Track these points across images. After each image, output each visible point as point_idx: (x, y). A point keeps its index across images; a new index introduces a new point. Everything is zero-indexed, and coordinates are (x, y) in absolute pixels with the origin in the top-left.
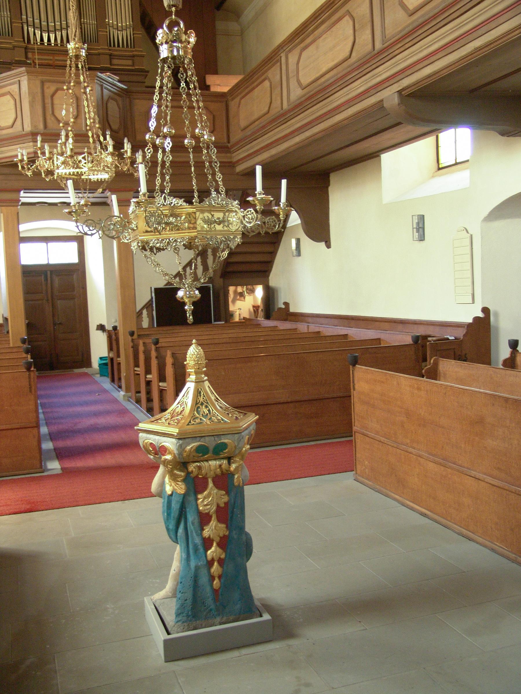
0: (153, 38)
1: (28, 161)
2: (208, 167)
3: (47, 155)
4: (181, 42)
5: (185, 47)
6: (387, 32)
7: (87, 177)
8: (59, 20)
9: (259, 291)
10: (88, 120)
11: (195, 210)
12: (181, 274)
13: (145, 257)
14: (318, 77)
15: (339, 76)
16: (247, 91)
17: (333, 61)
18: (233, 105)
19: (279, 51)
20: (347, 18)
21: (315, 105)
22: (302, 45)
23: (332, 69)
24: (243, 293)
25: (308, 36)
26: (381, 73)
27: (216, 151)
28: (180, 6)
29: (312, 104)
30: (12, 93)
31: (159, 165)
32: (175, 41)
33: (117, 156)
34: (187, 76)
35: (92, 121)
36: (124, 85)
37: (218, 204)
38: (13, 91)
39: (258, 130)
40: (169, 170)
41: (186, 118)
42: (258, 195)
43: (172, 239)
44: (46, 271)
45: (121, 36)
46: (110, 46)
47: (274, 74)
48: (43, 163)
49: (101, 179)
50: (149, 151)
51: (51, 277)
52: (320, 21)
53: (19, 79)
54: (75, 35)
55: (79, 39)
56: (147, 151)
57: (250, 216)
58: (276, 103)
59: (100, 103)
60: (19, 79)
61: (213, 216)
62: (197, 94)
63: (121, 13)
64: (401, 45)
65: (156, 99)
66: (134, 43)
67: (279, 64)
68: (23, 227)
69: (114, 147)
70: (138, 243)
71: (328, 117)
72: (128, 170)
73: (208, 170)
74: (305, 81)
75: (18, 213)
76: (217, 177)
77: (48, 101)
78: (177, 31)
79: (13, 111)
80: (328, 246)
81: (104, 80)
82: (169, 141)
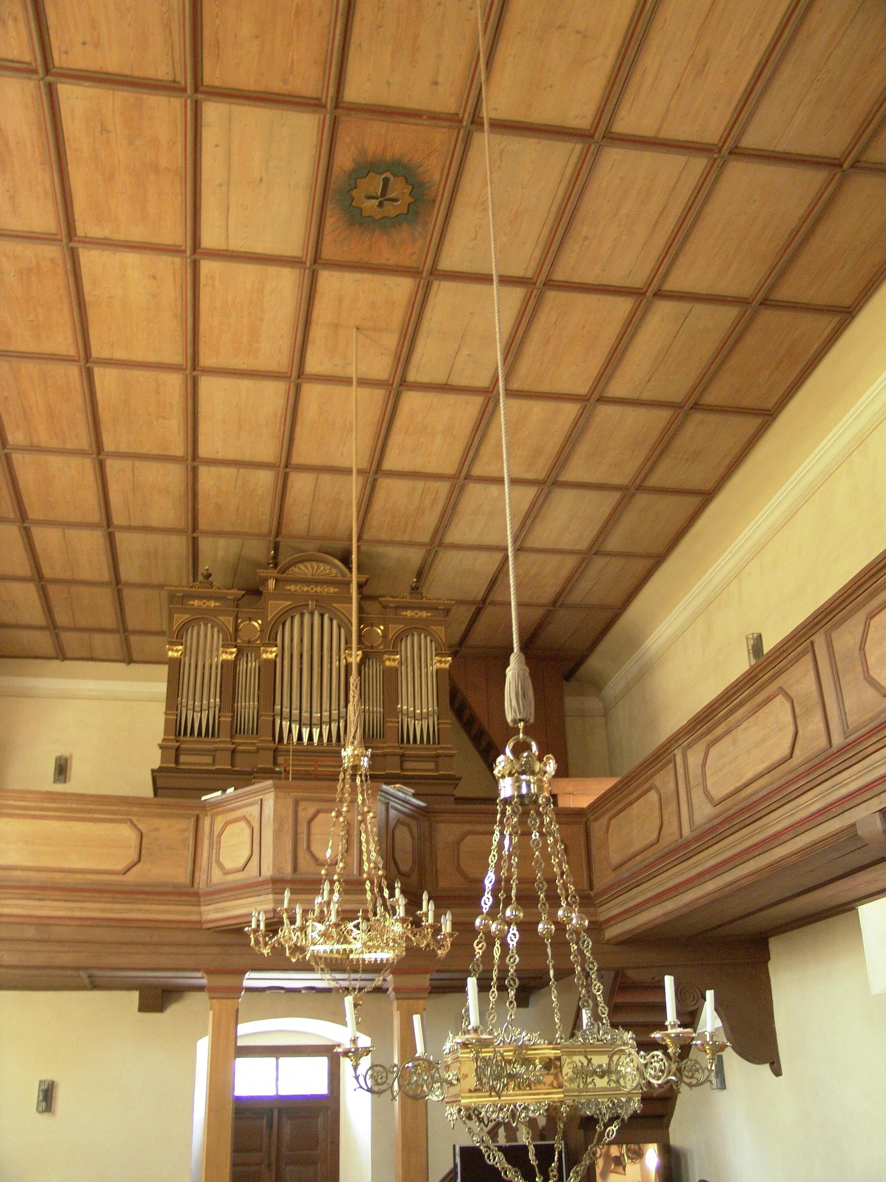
0: (491, 767)
1: (266, 931)
2: (579, 973)
3: (298, 923)
4: (533, 773)
5: (540, 781)
6: (850, 720)
7: (357, 956)
8: (328, 710)
9: (652, 1155)
10: (366, 863)
11: (559, 1051)
12: (533, 1166)
13: (470, 1132)
14: (738, 787)
15: (775, 786)
16: (620, 806)
17: (763, 762)
18: (597, 828)
19: (671, 746)
20: (780, 698)
21: (738, 831)
22: (709, 737)
23: (761, 776)
24: (622, 1159)
25: (719, 723)
26: (846, 782)
27: (591, 943)
28: (532, 721)
29: (732, 830)
30: (249, 819)
31: (496, 967)
32: (524, 773)
33: (412, 923)
34: (542, 823)
35: (372, 865)
36: (422, 801)
37: (598, 1040)
38: (251, 815)
39: (641, 871)
40: (514, 980)
41: (540, 889)
42: (669, 1027)
43: (520, 1106)
44: (272, 1110)
45: (419, 727)
46: (402, 741)
47: (664, 780)
48: (288, 934)
49: (382, 960)
50: (480, 946)
51: (279, 1121)
52: (735, 702)
53: (261, 797)
54: (354, 737)
55: (360, 743)
56: (477, 945)
57: (657, 1065)
58: (671, 828)
59: (384, 830)
60: (261, 797)
61: (589, 1061)
62: (558, 852)
63: (421, 693)
64: (877, 739)
65: (492, 861)
66: (438, 737)
67: (671, 765)
68: (243, 1029)
69: (407, 912)
70: (460, 1111)
71: (761, 850)
72: (428, 945)
73: (579, 979)
74: (718, 792)
75: (237, 1010)
76: (593, 988)
77: (303, 829)
78: (527, 757)
79: (248, 845)
80: (777, 1072)
81: (391, 795)
82: (515, 932)
